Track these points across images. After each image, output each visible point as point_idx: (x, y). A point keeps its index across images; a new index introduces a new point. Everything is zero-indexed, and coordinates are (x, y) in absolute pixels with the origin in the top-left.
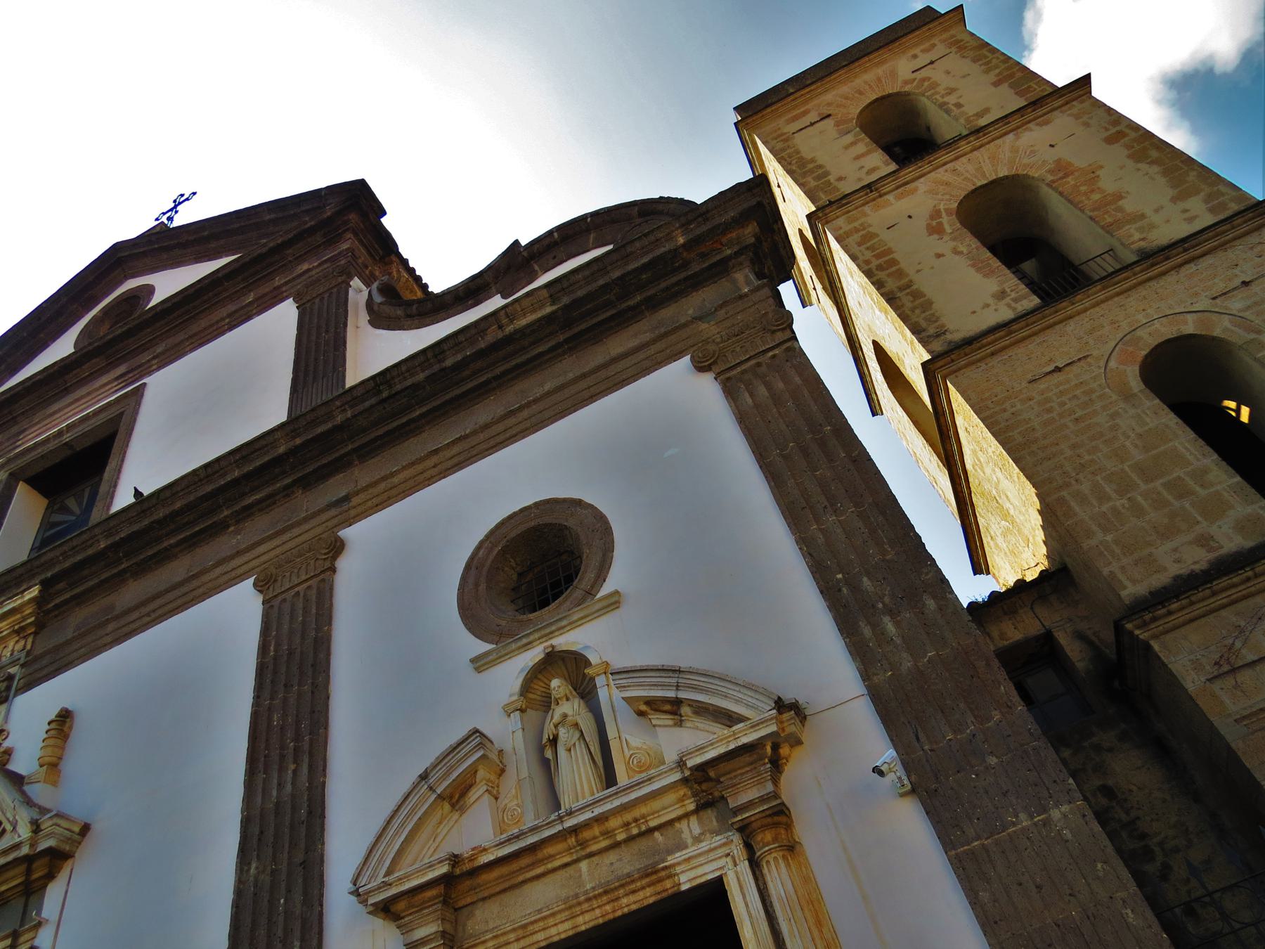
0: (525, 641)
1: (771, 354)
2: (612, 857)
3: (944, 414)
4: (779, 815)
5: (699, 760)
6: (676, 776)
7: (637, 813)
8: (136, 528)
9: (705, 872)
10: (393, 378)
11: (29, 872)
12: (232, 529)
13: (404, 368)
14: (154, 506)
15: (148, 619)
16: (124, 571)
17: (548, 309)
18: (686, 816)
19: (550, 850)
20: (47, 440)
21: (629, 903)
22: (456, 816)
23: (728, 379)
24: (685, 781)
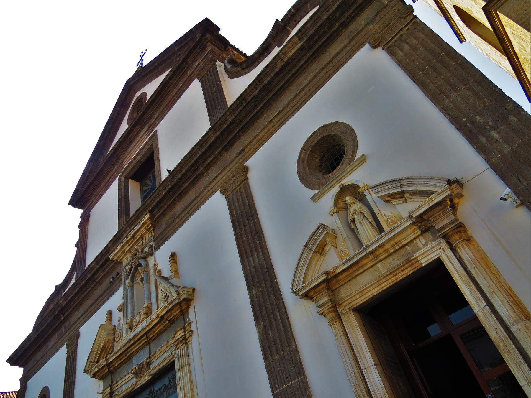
0: (330, 185)
1: (406, 28)
2: (390, 259)
3: (499, 29)
4: (460, 227)
5: (418, 214)
6: (410, 222)
7: (396, 240)
8: (172, 184)
9: (433, 257)
10: (245, 96)
11: (181, 307)
12: (205, 174)
13: (248, 91)
14: (176, 174)
15: (188, 215)
16: (174, 200)
17: (300, 45)
18: (418, 237)
19: (364, 262)
20: (132, 162)
21: (402, 275)
22: (323, 257)
23: (389, 47)
24: (414, 223)
